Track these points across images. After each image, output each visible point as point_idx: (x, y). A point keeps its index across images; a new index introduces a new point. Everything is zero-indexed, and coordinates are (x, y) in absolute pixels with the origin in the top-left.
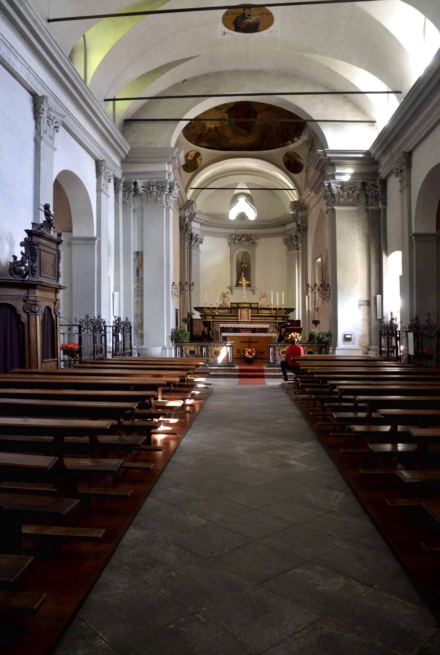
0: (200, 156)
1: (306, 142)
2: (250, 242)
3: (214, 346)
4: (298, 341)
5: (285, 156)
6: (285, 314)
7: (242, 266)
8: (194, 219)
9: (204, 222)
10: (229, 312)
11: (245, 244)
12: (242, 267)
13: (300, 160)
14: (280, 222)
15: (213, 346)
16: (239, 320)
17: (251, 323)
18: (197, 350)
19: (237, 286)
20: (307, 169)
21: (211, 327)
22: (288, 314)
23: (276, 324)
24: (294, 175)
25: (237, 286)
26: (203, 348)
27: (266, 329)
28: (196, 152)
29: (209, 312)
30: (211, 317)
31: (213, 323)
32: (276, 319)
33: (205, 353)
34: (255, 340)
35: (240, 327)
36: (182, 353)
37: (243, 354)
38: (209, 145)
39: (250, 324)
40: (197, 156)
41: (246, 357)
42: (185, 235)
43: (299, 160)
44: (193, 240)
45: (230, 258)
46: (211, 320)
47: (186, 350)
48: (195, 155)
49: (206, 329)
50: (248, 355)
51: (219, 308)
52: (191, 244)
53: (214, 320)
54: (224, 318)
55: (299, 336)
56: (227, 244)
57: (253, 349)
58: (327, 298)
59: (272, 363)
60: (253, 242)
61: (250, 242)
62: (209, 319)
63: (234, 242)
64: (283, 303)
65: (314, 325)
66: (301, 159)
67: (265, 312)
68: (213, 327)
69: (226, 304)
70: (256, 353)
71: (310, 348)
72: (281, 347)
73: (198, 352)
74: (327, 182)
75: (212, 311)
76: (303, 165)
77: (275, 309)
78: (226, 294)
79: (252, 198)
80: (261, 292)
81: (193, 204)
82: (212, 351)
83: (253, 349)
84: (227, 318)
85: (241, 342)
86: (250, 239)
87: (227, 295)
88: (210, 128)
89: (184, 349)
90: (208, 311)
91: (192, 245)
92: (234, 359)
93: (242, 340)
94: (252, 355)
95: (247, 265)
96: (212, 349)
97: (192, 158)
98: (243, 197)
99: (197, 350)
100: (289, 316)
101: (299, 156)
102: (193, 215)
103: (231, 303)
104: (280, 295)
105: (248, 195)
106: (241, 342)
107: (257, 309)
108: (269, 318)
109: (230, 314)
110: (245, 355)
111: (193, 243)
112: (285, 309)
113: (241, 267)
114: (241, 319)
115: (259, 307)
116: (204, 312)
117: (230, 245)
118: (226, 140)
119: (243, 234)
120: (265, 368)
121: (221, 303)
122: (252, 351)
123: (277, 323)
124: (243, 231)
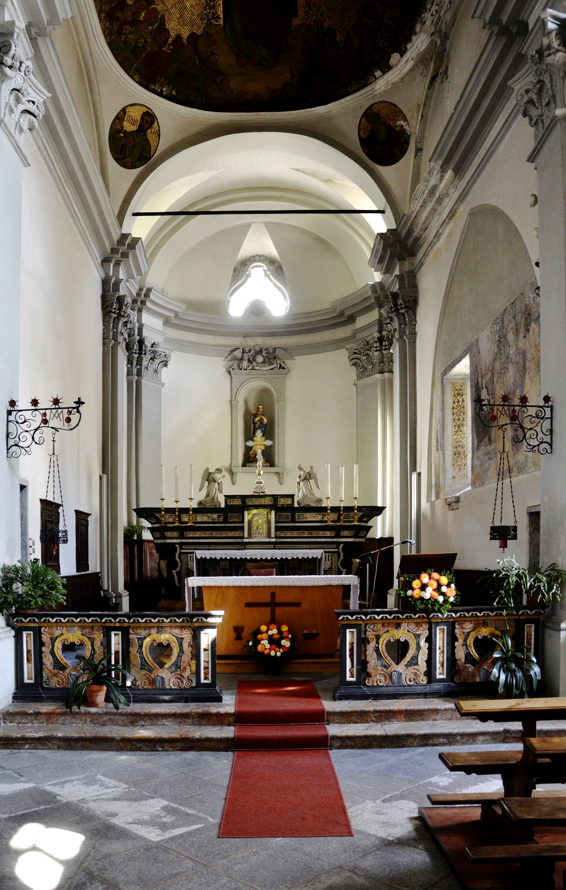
0: (156, 124)
1: (422, 60)
2: (275, 365)
3: (150, 628)
4: (445, 601)
5: (364, 119)
6: (360, 520)
7: (256, 420)
8: (148, 304)
9: (172, 315)
10: (221, 519)
11: (264, 369)
12: (256, 423)
13: (402, 123)
14: (342, 314)
15: (146, 628)
16: (245, 540)
17: (275, 546)
18: (92, 640)
19: (244, 465)
20: (419, 146)
21: (177, 559)
22: (367, 522)
23: (338, 548)
24: (385, 171)
25: (244, 465)
26: (113, 633)
27: (314, 560)
28: (145, 110)
29: (171, 520)
30: (175, 534)
31: (181, 548)
32: (338, 536)
33: (117, 653)
34: (291, 598)
35: (249, 558)
36: (41, 652)
37: (251, 643)
38: (177, 92)
39: (274, 548)
40: (147, 122)
41: (262, 653)
42: (117, 328)
43: (398, 123)
44: (145, 354)
45: (231, 402)
46: (175, 541)
47: (53, 640)
48: (142, 118)
49: (163, 564)
50: (268, 646)
51: (195, 511)
52: (141, 365)
53: (183, 541)
54: (208, 534)
55: (448, 586)
56: (224, 371)
57: (285, 628)
58: (542, 446)
59: (351, 683)
60: (281, 366)
61: (275, 365)
62: (172, 539)
63: (239, 366)
64: (356, 493)
65: (497, 543)
66: (405, 119)
67: (310, 517)
68: (180, 557)
69: (213, 499)
70: (292, 641)
71: (485, 624)
72: (383, 625)
73: (93, 649)
74: (555, 13)
75: (179, 517)
76: (409, 136)
77: (335, 509)
78: (214, 473)
79: (281, 267)
80: (303, 466)
81: (137, 246)
82: (141, 646)
83: (285, 628)
84: (215, 534)
85: (248, 605)
86: (275, 358)
87: (218, 476)
88: (179, 37)
89: (45, 638)
90: (169, 518)
91: (143, 367)
92: (221, 657)
93: (250, 599)
94: (280, 646)
95: (266, 417)
96: (141, 640)
97: (135, 128)
98: (260, 266)
99: (92, 640)
100: (371, 527)
101: (401, 112)
102: (145, 295)
103: (227, 497)
104: (349, 473)
105: (271, 261)
106: (248, 605)
107: (291, 509)
108: (321, 533)
109: (223, 525)
110: (260, 648)
111: (145, 363)
112: (360, 508)
113: (255, 423)
114: (250, 536)
115: (296, 505)
116: (159, 521)
117: (229, 372)
118: (218, 81)
119: (258, 349)
120: (329, 705)
121: (201, 496)
122: (280, 632)
123: (342, 545)
124: (259, 342)
